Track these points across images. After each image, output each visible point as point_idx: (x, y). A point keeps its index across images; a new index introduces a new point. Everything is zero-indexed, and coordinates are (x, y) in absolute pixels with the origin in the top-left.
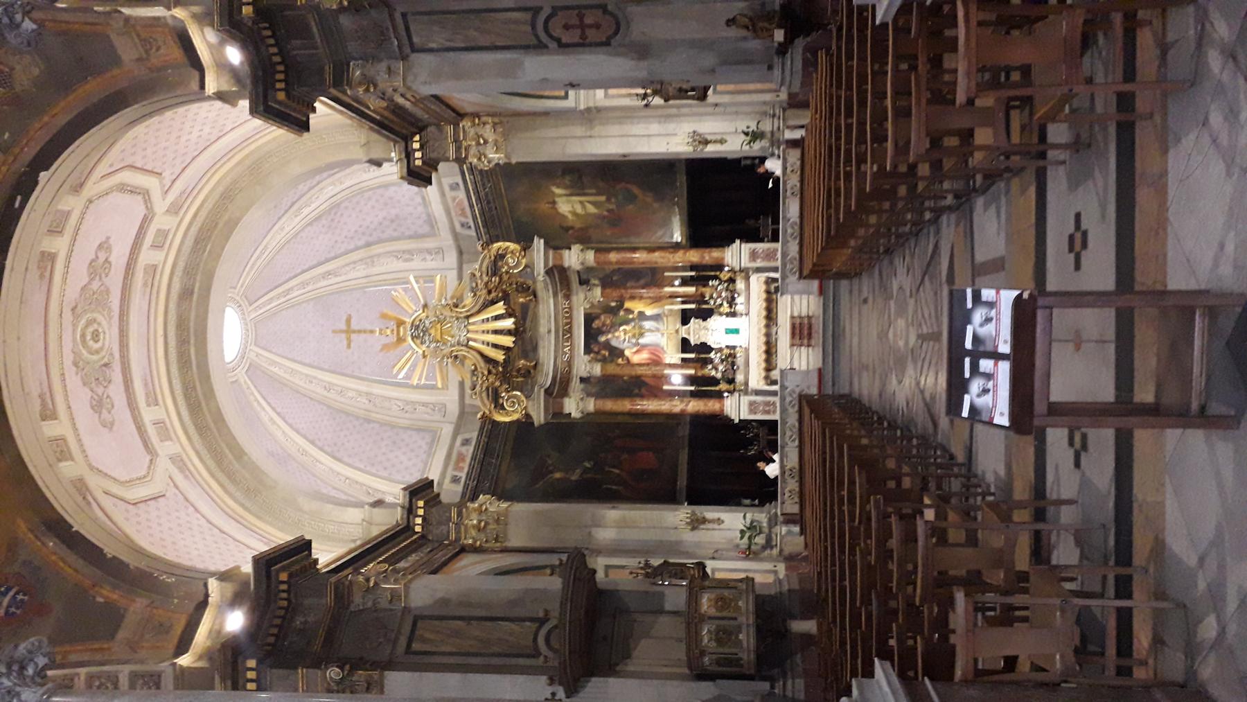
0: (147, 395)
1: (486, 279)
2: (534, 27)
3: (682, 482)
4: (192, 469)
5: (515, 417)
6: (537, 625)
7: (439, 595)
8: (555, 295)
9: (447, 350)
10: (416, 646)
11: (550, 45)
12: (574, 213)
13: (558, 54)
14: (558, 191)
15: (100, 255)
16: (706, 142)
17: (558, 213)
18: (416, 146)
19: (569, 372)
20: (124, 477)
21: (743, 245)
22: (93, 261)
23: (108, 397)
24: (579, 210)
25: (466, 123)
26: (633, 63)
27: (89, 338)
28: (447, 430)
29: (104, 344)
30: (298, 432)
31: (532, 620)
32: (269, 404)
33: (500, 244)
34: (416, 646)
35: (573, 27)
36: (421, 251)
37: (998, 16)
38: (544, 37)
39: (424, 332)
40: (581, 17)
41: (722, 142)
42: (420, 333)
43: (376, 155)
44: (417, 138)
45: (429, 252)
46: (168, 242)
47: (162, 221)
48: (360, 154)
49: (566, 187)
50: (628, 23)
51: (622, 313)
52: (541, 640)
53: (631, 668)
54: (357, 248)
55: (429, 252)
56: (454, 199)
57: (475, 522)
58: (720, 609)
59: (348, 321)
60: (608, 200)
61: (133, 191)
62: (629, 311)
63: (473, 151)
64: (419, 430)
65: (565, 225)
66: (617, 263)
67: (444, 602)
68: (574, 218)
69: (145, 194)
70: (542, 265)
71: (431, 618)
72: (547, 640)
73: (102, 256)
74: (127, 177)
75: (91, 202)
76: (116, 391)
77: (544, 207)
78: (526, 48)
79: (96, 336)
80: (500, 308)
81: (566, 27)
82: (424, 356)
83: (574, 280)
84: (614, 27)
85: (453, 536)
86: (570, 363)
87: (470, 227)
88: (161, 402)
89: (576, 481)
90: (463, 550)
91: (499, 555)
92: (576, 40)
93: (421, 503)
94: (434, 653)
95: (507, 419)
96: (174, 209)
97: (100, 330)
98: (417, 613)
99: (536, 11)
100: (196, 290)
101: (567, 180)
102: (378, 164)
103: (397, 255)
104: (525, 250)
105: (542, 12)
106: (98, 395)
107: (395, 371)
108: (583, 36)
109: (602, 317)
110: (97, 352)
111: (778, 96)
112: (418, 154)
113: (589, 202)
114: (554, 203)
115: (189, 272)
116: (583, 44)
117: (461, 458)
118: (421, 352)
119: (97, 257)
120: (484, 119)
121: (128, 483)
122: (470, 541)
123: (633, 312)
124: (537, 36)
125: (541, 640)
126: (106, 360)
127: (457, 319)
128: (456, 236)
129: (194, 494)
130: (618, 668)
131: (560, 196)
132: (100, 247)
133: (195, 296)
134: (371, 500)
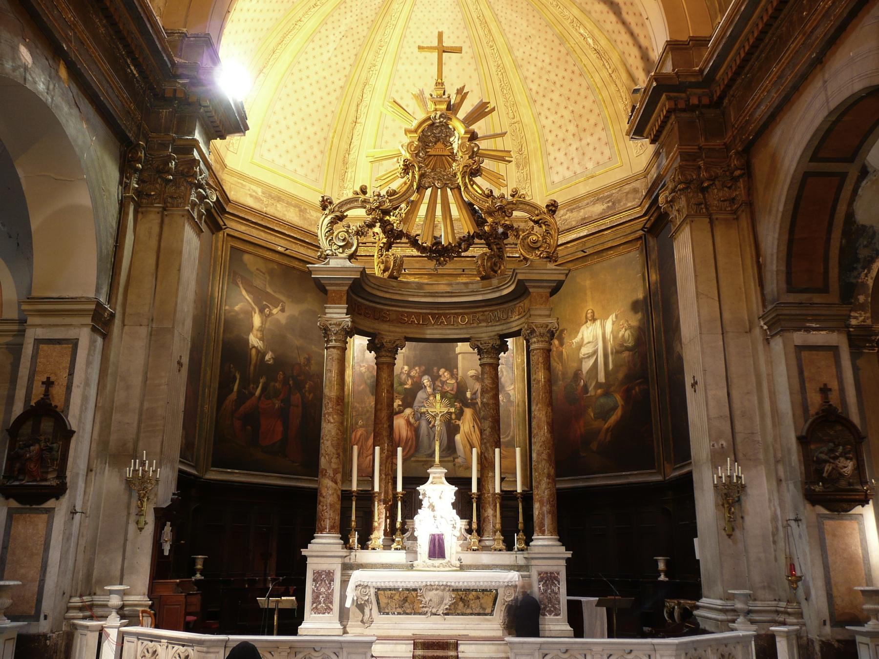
12: (580, 346)
17: (580, 326)
21: (564, 563)
24: (585, 351)
37: (348, 609)
60: (599, 385)
68: (574, 346)
77: (590, 307)
89: (248, 340)
109: (453, 381)
111: (46, 617)
113: (596, 360)
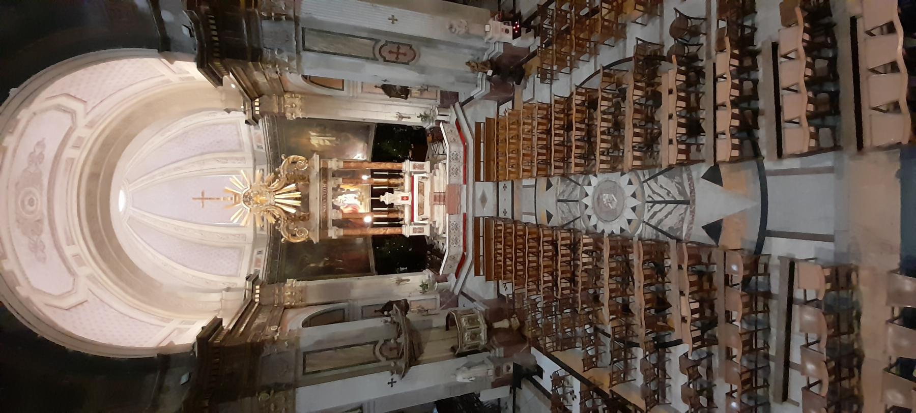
0: (67, 239)
1: (286, 173)
2: (374, 48)
3: (372, 263)
4: (101, 281)
5: (302, 240)
6: (373, 345)
7: (316, 339)
8: (320, 181)
9: (264, 208)
10: (308, 370)
11: (380, 60)
13: (383, 64)
14: (312, 134)
15: (37, 150)
16: (403, 117)
17: (311, 144)
18: (257, 104)
19: (327, 217)
20: (57, 292)
22: (32, 153)
23: (41, 241)
25: (287, 96)
26: (418, 74)
27: (26, 203)
28: (248, 248)
29: (37, 207)
30: (161, 253)
31: (371, 343)
32: (142, 239)
33: (293, 156)
34: (308, 370)
35: (393, 52)
36: (232, 158)
38: (378, 56)
39: (250, 199)
40: (398, 48)
41: (409, 118)
42: (247, 199)
43: (229, 107)
44: (257, 100)
45: (237, 159)
46: (83, 145)
47: (81, 131)
48: (220, 105)
49: (317, 132)
50: (419, 56)
51: (339, 190)
52: (377, 353)
53: (424, 358)
54: (195, 156)
55: (237, 159)
56: (256, 133)
57: (289, 293)
58: (471, 324)
59: (203, 194)
60: (337, 140)
61: (65, 110)
62: (342, 189)
63: (288, 110)
64: (232, 248)
65: (313, 149)
66: (354, 167)
67: (319, 342)
69: (72, 113)
70: (318, 167)
71: (313, 352)
72: (381, 353)
73: (38, 151)
74: (64, 101)
75: (35, 114)
76: (46, 238)
77: (304, 141)
78: (367, 59)
79: (31, 202)
80: (292, 186)
81: (390, 52)
82: (250, 211)
83: (330, 174)
84: (413, 56)
85: (277, 302)
86: (326, 213)
87: (262, 148)
88: (76, 243)
90: (286, 308)
91: (305, 308)
92: (394, 59)
93: (258, 287)
94: (319, 372)
95: (298, 241)
96: (91, 125)
97: (34, 198)
98: (305, 351)
99: (377, 41)
100: (102, 174)
101: (318, 129)
102: (228, 111)
103: (217, 160)
104: (308, 160)
105: (380, 43)
106: (33, 240)
107: (232, 219)
108: (397, 58)
110: (32, 212)
112: (257, 109)
114: (310, 139)
115: (97, 163)
116: (396, 62)
117: (258, 261)
118: (249, 209)
119: (35, 151)
120: (297, 95)
121: (61, 297)
122: (289, 303)
123: (344, 190)
124: (374, 55)
125: (377, 353)
126: (38, 218)
127: (270, 192)
128: (254, 152)
129: (106, 297)
130: (420, 359)
131: (313, 136)
132: (38, 144)
133: (101, 177)
134: (225, 287)
